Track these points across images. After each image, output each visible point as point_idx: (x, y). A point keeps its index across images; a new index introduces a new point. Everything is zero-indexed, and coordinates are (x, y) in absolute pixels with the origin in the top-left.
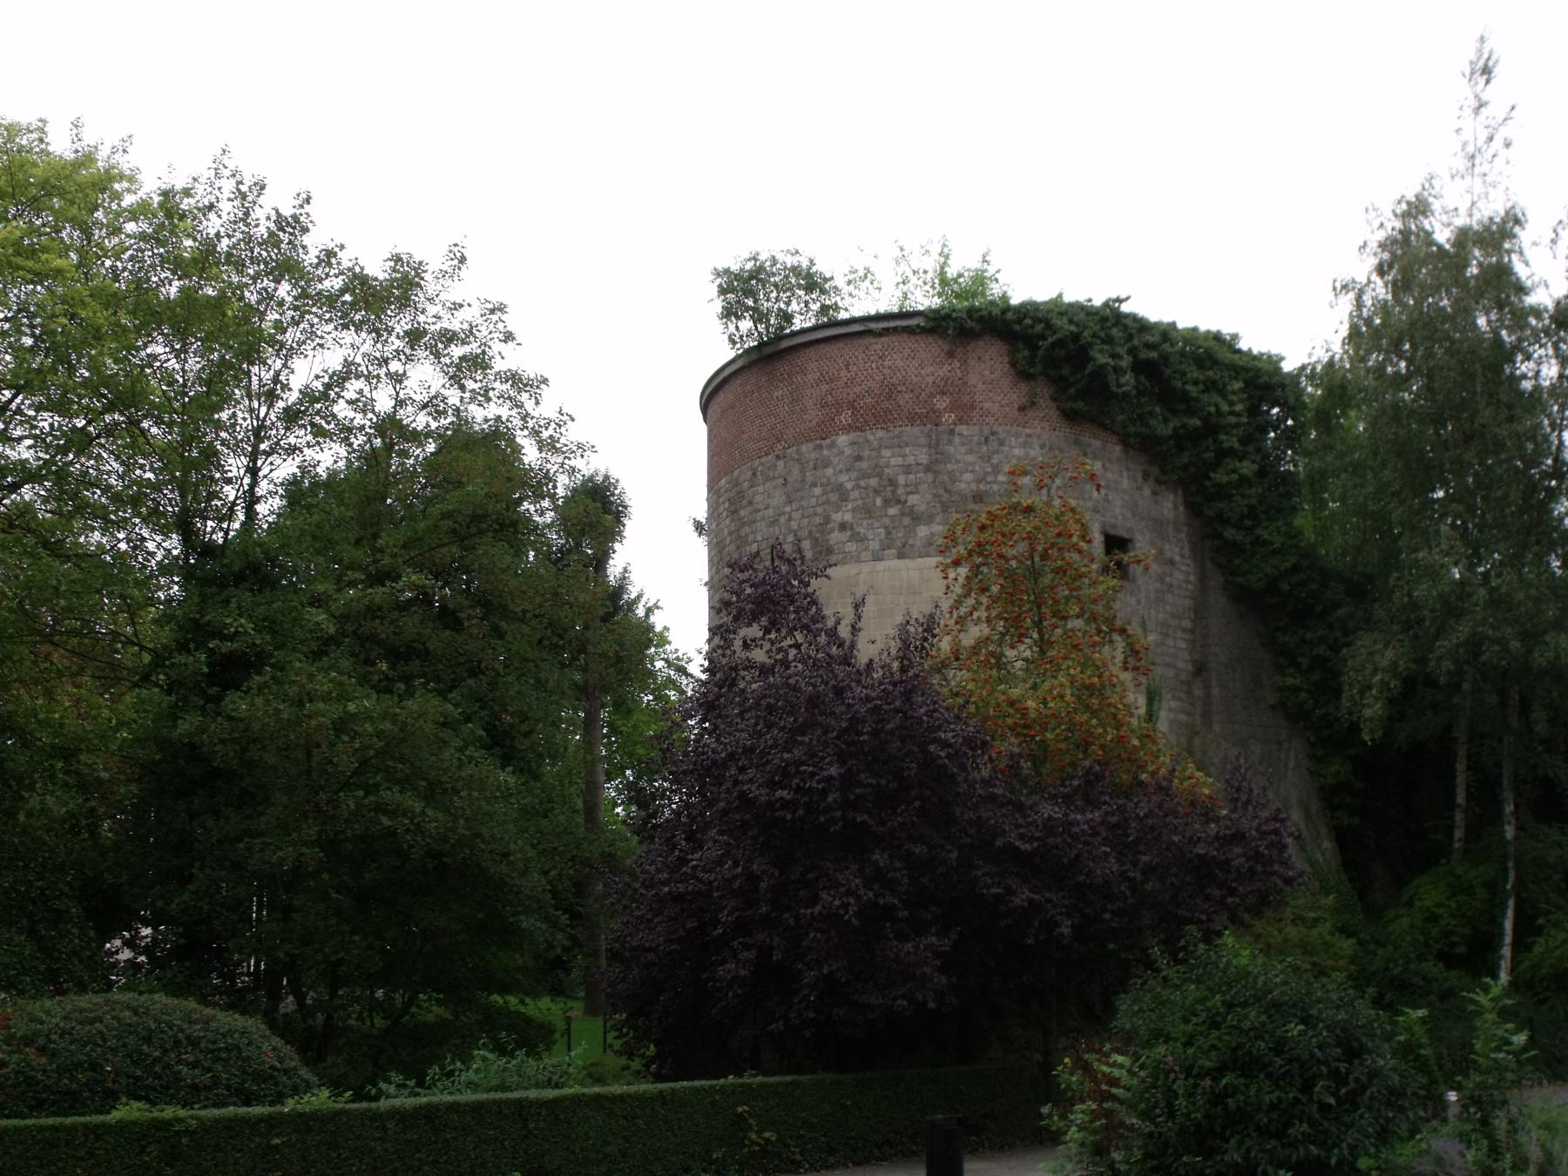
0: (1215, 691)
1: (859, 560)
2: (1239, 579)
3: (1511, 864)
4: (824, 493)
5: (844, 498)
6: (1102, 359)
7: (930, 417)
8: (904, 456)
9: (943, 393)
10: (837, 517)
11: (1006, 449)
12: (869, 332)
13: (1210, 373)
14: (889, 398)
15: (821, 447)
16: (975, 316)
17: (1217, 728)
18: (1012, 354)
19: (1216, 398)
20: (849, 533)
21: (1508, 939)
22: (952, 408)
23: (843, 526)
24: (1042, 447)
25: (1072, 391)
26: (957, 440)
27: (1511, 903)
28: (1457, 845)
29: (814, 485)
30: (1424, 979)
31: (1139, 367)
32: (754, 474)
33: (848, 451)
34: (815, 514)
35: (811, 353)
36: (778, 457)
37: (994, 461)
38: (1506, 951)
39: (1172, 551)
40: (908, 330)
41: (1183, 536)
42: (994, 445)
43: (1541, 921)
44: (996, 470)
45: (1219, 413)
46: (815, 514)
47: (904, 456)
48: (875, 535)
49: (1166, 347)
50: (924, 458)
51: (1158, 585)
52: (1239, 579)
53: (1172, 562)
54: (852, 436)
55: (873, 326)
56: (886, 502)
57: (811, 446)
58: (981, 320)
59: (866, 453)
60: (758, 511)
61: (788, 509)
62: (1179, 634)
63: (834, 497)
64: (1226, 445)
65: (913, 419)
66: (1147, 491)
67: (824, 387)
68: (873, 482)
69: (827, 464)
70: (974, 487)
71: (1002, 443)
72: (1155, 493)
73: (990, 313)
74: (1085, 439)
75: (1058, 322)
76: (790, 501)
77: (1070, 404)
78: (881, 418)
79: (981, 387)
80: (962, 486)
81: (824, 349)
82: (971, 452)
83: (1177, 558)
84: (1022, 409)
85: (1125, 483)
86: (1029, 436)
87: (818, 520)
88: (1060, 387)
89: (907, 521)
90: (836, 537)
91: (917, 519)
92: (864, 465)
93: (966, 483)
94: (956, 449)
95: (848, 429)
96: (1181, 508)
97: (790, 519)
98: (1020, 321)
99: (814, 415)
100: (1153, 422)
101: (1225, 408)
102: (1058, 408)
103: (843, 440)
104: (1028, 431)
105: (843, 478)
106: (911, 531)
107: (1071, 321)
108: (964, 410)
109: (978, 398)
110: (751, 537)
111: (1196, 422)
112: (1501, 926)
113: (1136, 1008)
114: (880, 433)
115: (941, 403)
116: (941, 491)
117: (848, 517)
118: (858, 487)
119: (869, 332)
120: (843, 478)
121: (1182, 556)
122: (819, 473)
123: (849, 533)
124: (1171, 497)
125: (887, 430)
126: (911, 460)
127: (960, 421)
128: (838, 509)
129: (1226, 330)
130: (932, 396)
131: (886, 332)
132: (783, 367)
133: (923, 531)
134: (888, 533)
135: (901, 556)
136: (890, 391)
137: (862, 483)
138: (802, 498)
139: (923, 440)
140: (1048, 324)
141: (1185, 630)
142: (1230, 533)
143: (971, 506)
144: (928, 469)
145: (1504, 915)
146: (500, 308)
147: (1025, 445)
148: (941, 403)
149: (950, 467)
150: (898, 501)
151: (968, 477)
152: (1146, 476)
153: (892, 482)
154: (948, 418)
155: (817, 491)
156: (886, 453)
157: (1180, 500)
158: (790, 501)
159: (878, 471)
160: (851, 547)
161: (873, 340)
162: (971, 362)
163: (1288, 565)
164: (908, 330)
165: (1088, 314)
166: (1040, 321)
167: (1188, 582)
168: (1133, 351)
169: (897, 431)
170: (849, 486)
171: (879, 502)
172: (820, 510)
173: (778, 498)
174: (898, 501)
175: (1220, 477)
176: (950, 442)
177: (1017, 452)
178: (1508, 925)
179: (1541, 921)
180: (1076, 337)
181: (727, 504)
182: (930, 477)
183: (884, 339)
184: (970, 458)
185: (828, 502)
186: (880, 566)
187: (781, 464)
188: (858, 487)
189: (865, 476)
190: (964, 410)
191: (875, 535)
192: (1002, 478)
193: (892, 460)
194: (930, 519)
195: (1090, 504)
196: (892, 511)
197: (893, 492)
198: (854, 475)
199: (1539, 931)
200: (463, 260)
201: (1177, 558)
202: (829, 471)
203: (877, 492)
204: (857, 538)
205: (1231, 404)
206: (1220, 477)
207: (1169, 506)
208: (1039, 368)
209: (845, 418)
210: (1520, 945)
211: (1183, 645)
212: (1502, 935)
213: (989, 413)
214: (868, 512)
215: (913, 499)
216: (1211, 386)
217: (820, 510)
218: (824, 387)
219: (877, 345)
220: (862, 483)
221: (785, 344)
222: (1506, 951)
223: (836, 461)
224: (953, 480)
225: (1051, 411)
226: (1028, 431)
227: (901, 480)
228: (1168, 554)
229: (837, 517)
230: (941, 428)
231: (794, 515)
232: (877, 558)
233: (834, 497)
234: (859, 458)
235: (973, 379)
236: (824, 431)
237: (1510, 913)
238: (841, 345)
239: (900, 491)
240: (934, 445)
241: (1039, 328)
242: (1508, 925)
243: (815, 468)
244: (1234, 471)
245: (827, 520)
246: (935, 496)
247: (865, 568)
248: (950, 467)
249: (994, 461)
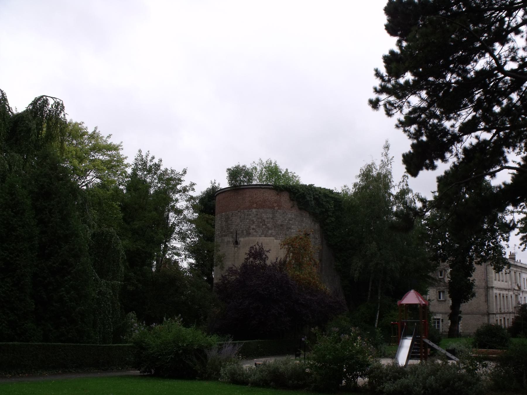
0: (323, 266)
1: (256, 236)
2: (330, 243)
3: (379, 304)
4: (249, 221)
5: (254, 223)
6: (308, 199)
7: (273, 208)
8: (267, 215)
9: (275, 203)
10: (252, 227)
11: (287, 215)
12: (261, 188)
13: (327, 199)
15: (249, 211)
16: (284, 187)
17: (323, 273)
19: (328, 205)
20: (254, 230)
21: (377, 318)
22: (278, 206)
23: (253, 229)
24: (294, 215)
26: (278, 213)
27: (378, 311)
28: (368, 299)
29: (247, 219)
30: (9, 109)
31: (315, 199)
32: (233, 214)
33: (255, 213)
34: (247, 225)
36: (239, 212)
37: (285, 218)
38: (377, 321)
39: (317, 236)
40: (269, 188)
41: (319, 233)
43: (384, 315)
44: (285, 220)
45: (329, 208)
46: (247, 225)
47: (267, 215)
49: (320, 195)
50: (271, 216)
51: (314, 243)
52: (330, 243)
53: (317, 238)
55: (262, 187)
57: (247, 210)
59: (259, 214)
60: (233, 222)
61: (241, 223)
62: (317, 254)
63: (251, 222)
64: (329, 215)
65: (269, 208)
66: (313, 224)
68: (260, 220)
69: (250, 215)
70: (281, 223)
71: (287, 214)
72: (314, 224)
73: (287, 187)
76: (241, 222)
79: (283, 202)
80: (279, 223)
82: (280, 216)
83: (318, 238)
84: (292, 207)
85: (309, 222)
86: (292, 213)
87: (248, 227)
89: (267, 229)
90: (251, 231)
91: (269, 229)
92: (258, 216)
93: (279, 222)
95: (255, 208)
96: (319, 227)
97: (241, 226)
100: (316, 210)
101: (330, 207)
102: (298, 207)
103: (254, 210)
104: (292, 212)
105: (254, 218)
107: (303, 190)
108: (280, 207)
110: (231, 228)
113: (37, 347)
114: (262, 210)
115: (275, 205)
116: (274, 224)
117: (254, 227)
118: (257, 221)
119: (261, 188)
120: (254, 218)
121: (319, 237)
123: (254, 230)
124: (317, 224)
125: (264, 209)
126: (268, 216)
127: (279, 209)
128: (252, 225)
131: (265, 188)
133: (270, 232)
134: (263, 231)
135: (265, 236)
137: (258, 220)
138: (244, 221)
140: (298, 191)
141: (318, 253)
142: (328, 233)
144: (272, 219)
145: (377, 314)
146: (194, 184)
147: (291, 215)
148: (275, 205)
149: (276, 218)
150: (265, 225)
152: (313, 220)
153: (264, 221)
155: (248, 220)
156: (263, 214)
157: (319, 225)
158: (241, 222)
160: (255, 233)
161: (262, 189)
162: (282, 196)
163: (340, 240)
164: (269, 188)
165: (306, 188)
166: (296, 189)
167: (319, 242)
168: (314, 196)
169: (266, 210)
170: (255, 220)
171: (261, 225)
173: (238, 221)
174: (265, 225)
175: (328, 221)
176: (276, 213)
177: (289, 216)
178: (378, 316)
179: (384, 315)
180: (303, 193)
181: (224, 219)
182: (272, 220)
183: (264, 190)
184: (280, 217)
185: (250, 223)
186: (261, 238)
187: (239, 213)
188: (257, 221)
189: (258, 219)
190: (280, 207)
192: (286, 221)
193: (264, 216)
194: (272, 229)
195: (303, 227)
196: (264, 227)
197: (264, 223)
198: (256, 218)
200: (186, 172)
201: (318, 238)
202: (251, 217)
204: (256, 232)
205: (331, 206)
206: (328, 221)
207: (317, 226)
209: (255, 205)
210: (380, 319)
211: (317, 256)
212: (376, 317)
214: (259, 227)
215: (268, 225)
216: (328, 202)
219: (262, 191)
220: (258, 220)
221: (242, 187)
222: (377, 321)
223: (252, 214)
226: (292, 212)
227: (266, 220)
228: (316, 237)
229: (252, 227)
230: (275, 210)
231: (242, 225)
232: (260, 236)
233: (251, 222)
234: (257, 215)
236: (250, 208)
237: (378, 313)
238: (254, 189)
239: (266, 223)
241: (296, 191)
242: (378, 316)
243: (247, 215)
244: (330, 220)
245: (250, 227)
246: (273, 224)
247: (258, 238)
248: (276, 218)
249: (285, 218)
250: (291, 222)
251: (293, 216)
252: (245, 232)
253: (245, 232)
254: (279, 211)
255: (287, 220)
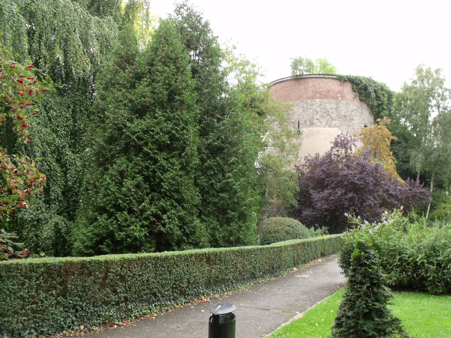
5: (317, 113)
7: (336, 98)
9: (339, 93)
10: (316, 117)
12: (325, 78)
14: (328, 92)
18: (353, 86)
21: (428, 211)
23: (317, 119)
25: (363, 95)
26: (341, 103)
27: (430, 204)
29: (310, 109)
33: (319, 103)
35: (310, 80)
36: (301, 101)
40: (333, 79)
42: (348, 105)
48: (324, 122)
50: (335, 107)
54: (320, 100)
55: (326, 76)
56: (327, 115)
57: (310, 100)
58: (348, 79)
59: (323, 104)
63: (315, 113)
65: (333, 98)
67: (313, 88)
68: (324, 110)
74: (363, 105)
75: (363, 81)
76: (304, 112)
77: (362, 98)
78: (326, 97)
81: (313, 79)
87: (311, 117)
88: (360, 94)
89: (331, 120)
90: (315, 121)
92: (322, 106)
93: (343, 113)
94: (341, 105)
95: (319, 98)
98: (355, 80)
99: (310, 94)
103: (317, 100)
105: (317, 109)
106: (331, 122)
108: (343, 97)
109: (346, 95)
111: (380, 103)
112: (427, 208)
114: (326, 100)
115: (339, 95)
117: (318, 117)
119: (325, 78)
120: (317, 109)
122: (312, 107)
126: (332, 107)
127: (342, 99)
128: (316, 115)
129: (384, 82)
130: (337, 93)
132: (302, 81)
134: (327, 122)
135: (329, 127)
136: (328, 91)
139: (335, 103)
143: (344, 118)
144: (336, 109)
147: (353, 106)
148: (339, 95)
151: (343, 112)
153: (328, 111)
154: (340, 99)
155: (311, 110)
156: (327, 105)
158: (304, 112)
159: (325, 108)
160: (319, 124)
162: (345, 87)
164: (333, 79)
170: (319, 110)
171: (325, 115)
172: (312, 115)
173: (301, 111)
178: (429, 208)
182: (336, 111)
184: (344, 108)
186: (325, 128)
187: (302, 103)
189: (322, 109)
191: (324, 122)
192: (349, 112)
194: (336, 120)
196: (328, 117)
199: (435, 209)
202: (314, 107)
203: (325, 113)
204: (320, 122)
208: (357, 90)
209: (318, 95)
213: (347, 99)
214: (323, 117)
215: (332, 115)
217: (312, 115)
218: (313, 88)
221: (304, 77)
224: (340, 112)
225: (358, 98)
227: (330, 111)
232: (324, 127)
234: (321, 105)
235: (345, 91)
236: (313, 98)
237: (429, 206)
239: (330, 113)
240: (337, 104)
245: (313, 117)
250: (353, 113)
251: (355, 108)
252: (308, 122)
253: (308, 122)
254: (342, 101)
255: (350, 110)
